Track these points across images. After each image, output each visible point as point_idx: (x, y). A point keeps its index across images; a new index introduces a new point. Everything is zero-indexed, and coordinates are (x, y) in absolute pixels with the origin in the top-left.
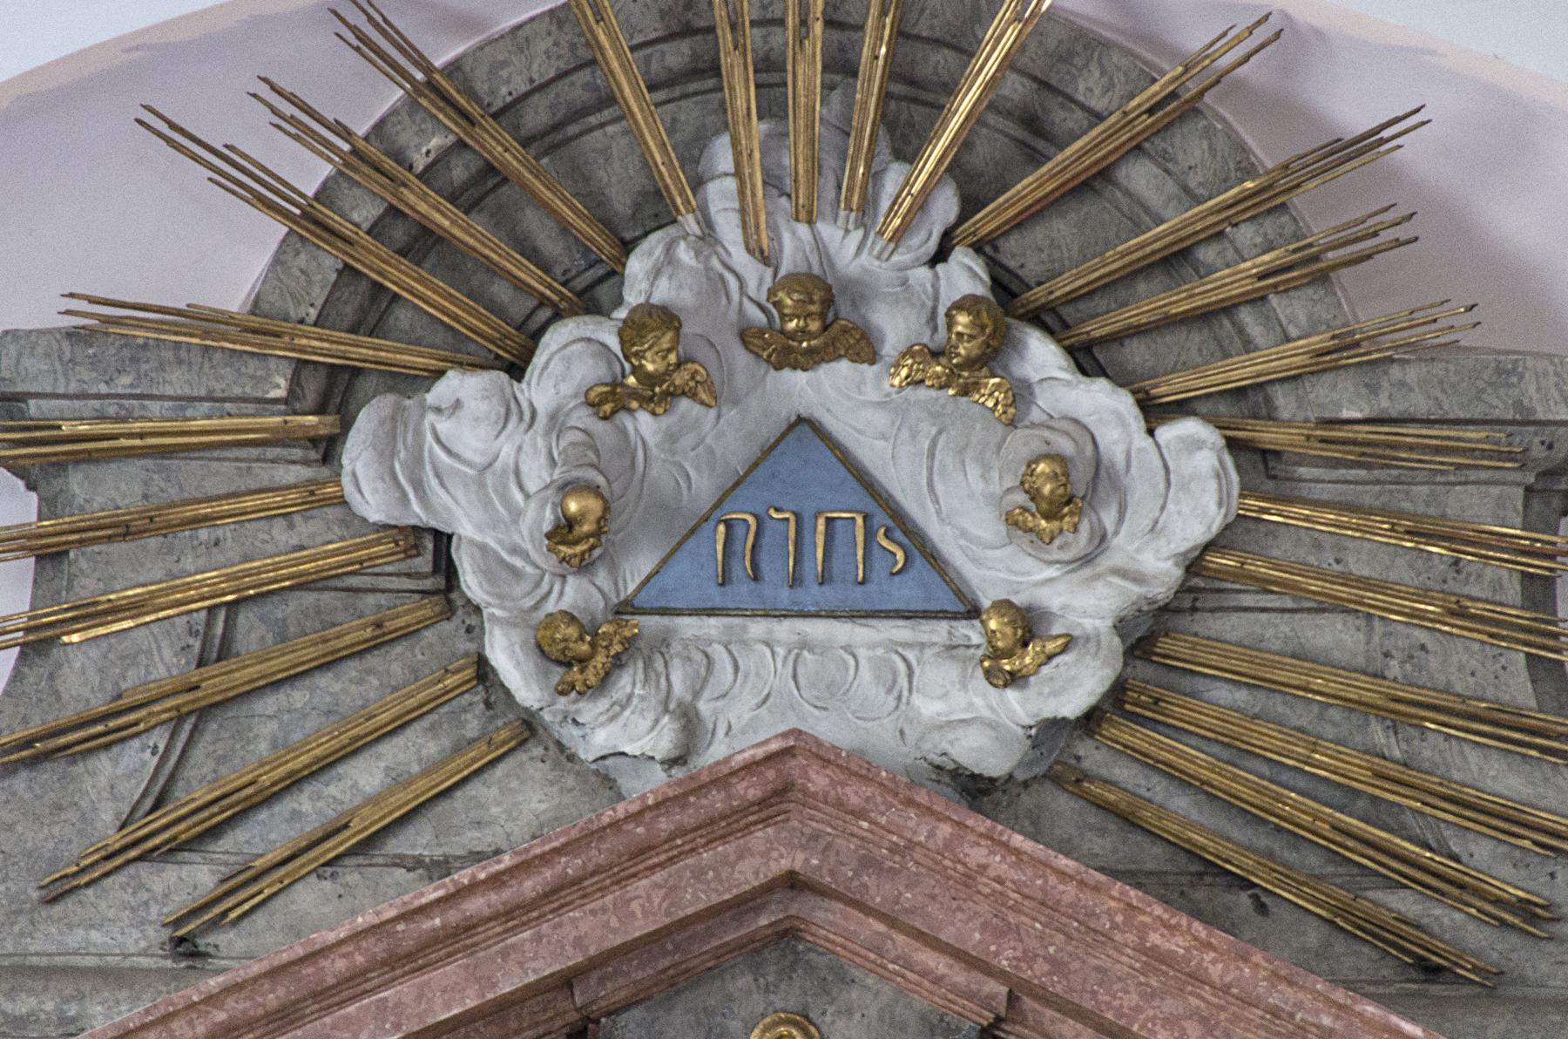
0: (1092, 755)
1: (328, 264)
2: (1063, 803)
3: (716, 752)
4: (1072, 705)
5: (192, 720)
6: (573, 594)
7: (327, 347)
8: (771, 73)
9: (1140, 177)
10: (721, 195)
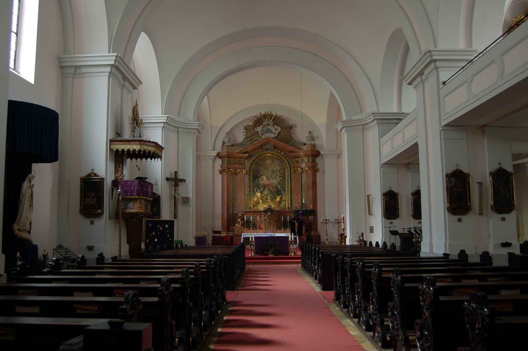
0: (277, 137)
1: (254, 123)
2: (276, 139)
3: (266, 137)
4: (276, 136)
5: (61, 253)
6: (262, 133)
7: (254, 126)
8: (267, 118)
9: (278, 120)
10: (266, 121)
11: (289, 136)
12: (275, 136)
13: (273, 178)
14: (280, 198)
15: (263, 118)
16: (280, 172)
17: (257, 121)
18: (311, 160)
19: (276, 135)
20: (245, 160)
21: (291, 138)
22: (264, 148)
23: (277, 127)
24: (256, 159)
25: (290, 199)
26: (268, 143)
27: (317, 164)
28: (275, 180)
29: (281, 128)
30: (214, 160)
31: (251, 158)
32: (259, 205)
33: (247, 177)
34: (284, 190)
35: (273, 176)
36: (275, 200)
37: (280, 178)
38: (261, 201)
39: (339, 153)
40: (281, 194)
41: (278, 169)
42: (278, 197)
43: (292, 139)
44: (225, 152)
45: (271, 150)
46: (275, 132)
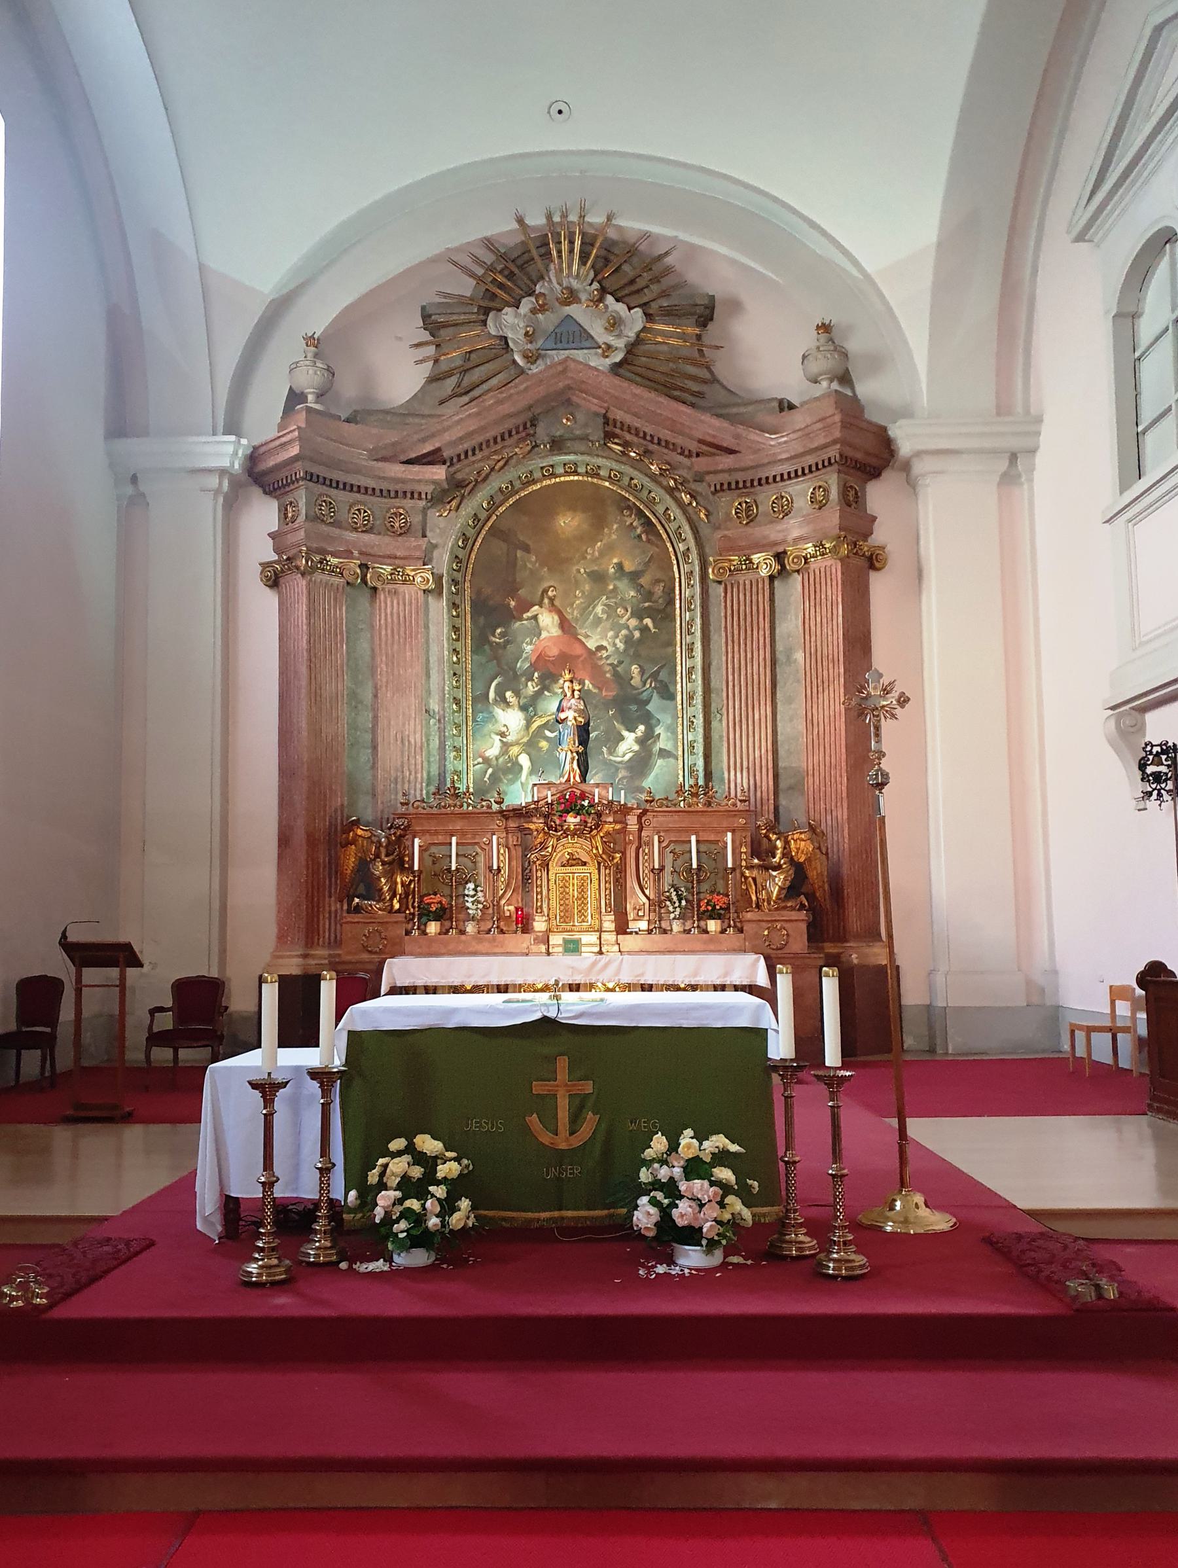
4: (618, 359)
10: (552, 274)
11: (694, 363)
12: (608, 361)
13: (598, 621)
14: (641, 741)
15: (536, 257)
16: (639, 588)
17: (501, 272)
18: (834, 494)
19: (618, 357)
20: (430, 512)
21: (703, 373)
22: (541, 431)
23: (621, 308)
24: (493, 505)
25: (699, 748)
26: (569, 402)
27: (874, 519)
28: (611, 634)
29: (649, 316)
30: (232, 503)
31: (463, 497)
32: (512, 782)
33: (439, 609)
34: (667, 694)
35: (599, 609)
36: (612, 751)
37: (641, 619)
38: (524, 760)
39: (1015, 443)
40: (648, 720)
41: (629, 567)
42: (625, 733)
43: (714, 380)
44: (290, 442)
45: (583, 448)
46: (611, 340)
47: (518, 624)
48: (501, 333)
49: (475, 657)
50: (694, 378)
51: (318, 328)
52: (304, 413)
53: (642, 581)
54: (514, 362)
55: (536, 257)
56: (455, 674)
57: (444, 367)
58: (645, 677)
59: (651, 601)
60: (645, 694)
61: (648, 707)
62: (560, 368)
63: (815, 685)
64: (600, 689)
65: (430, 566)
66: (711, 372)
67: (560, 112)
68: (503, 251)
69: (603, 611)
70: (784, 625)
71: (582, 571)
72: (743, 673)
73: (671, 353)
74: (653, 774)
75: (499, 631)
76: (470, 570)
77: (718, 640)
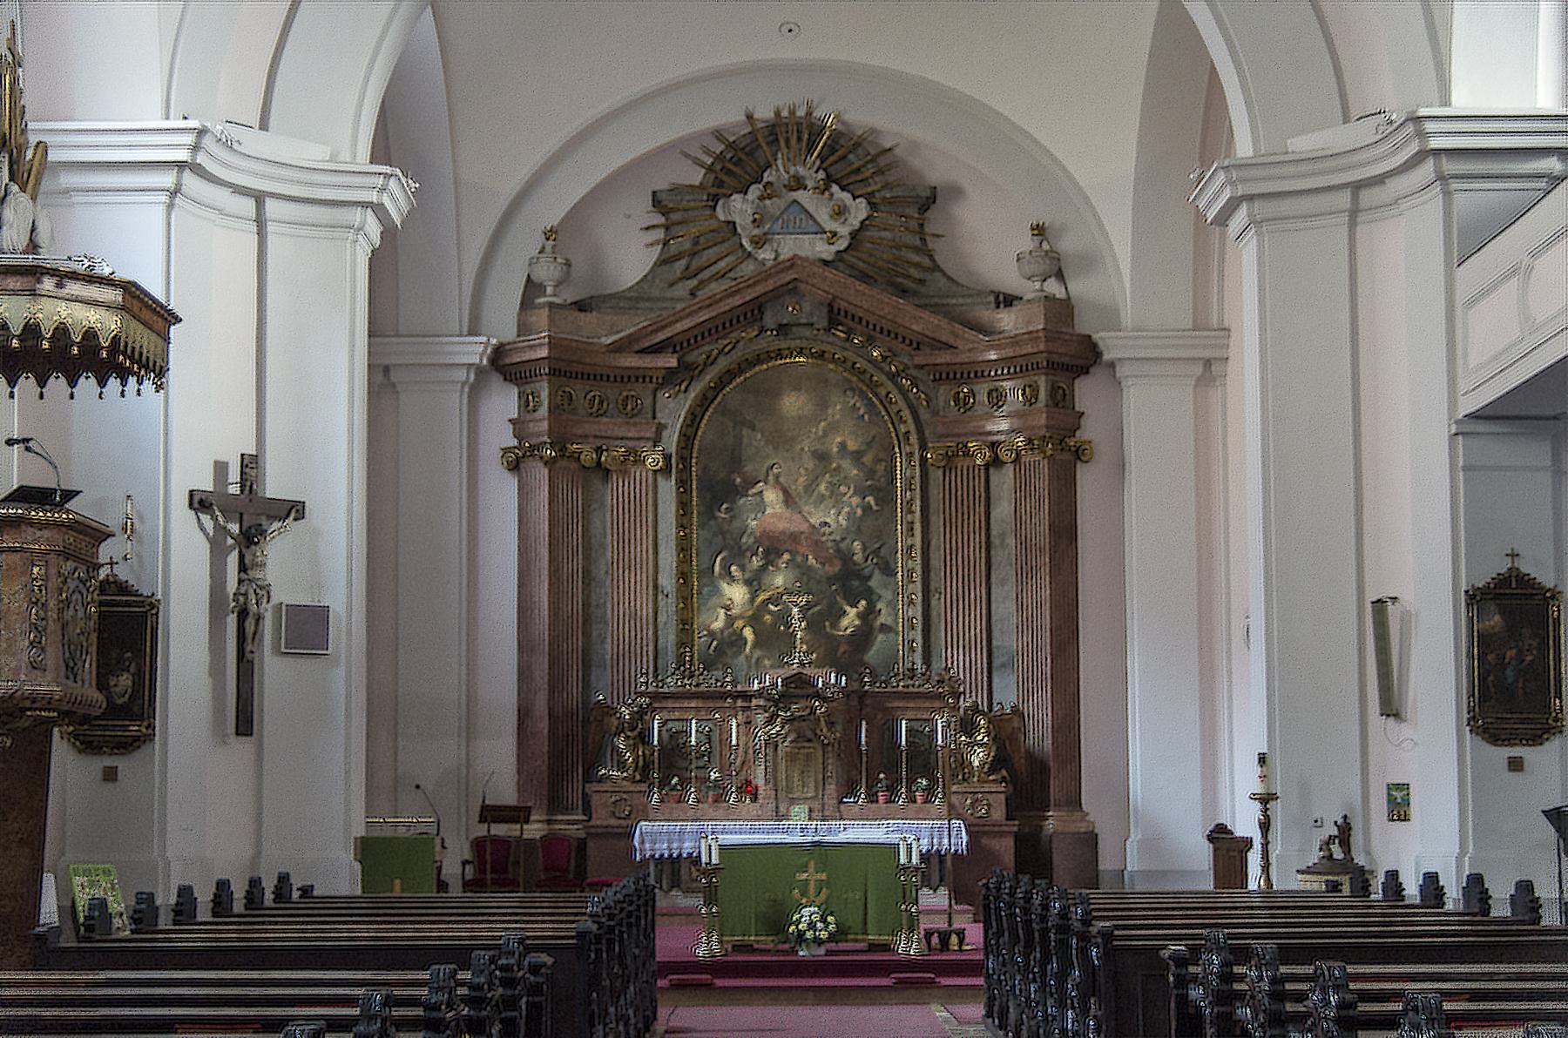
11: (917, 249)
12: (834, 248)
14: (862, 616)
15: (763, 145)
18: (1042, 395)
19: (842, 244)
21: (926, 261)
23: (846, 196)
29: (873, 206)
30: (475, 392)
33: (668, 489)
34: (889, 571)
35: (822, 487)
36: (835, 625)
38: (748, 633)
41: (852, 445)
42: (848, 608)
43: (936, 268)
44: (540, 345)
47: (744, 499)
48: (730, 219)
49: (701, 533)
50: (917, 265)
51: (553, 220)
52: (547, 309)
53: (865, 459)
54: (742, 245)
55: (763, 145)
56: (683, 549)
57: (674, 247)
58: (866, 554)
59: (873, 479)
60: (866, 570)
61: (870, 584)
62: (788, 264)
63: (1025, 572)
64: (823, 564)
65: (661, 448)
66: (933, 261)
67: (790, 31)
68: (731, 139)
69: (827, 488)
70: (998, 511)
71: (806, 449)
72: (960, 555)
73: (894, 241)
74: (874, 648)
75: (724, 506)
76: (696, 447)
77: (937, 521)
